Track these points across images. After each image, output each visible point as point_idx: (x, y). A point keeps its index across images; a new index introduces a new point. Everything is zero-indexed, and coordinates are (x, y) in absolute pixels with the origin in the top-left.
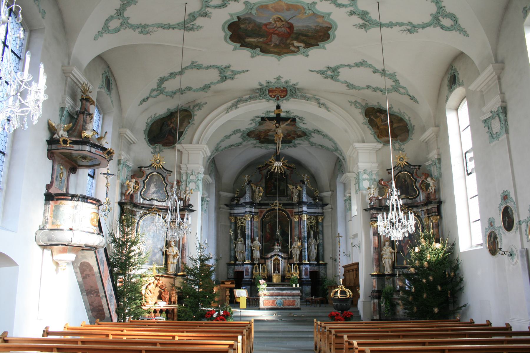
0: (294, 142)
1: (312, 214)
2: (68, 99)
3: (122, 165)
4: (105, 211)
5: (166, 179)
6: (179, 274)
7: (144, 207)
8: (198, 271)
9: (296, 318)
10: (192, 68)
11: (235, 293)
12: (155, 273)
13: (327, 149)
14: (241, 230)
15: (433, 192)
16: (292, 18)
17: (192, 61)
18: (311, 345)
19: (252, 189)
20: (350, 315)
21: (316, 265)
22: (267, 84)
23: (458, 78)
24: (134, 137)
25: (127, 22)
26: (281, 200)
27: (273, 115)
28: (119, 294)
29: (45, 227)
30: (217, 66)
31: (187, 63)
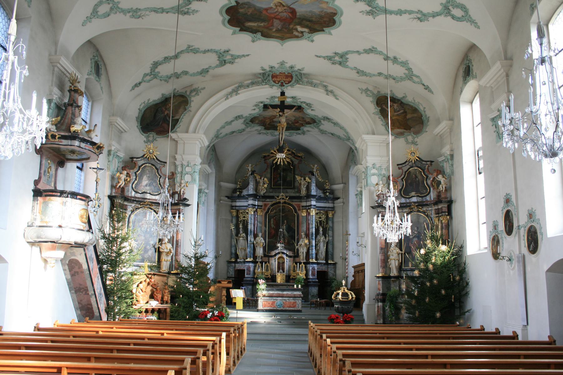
0: (303, 129)
1: (322, 209)
2: (56, 90)
3: (112, 155)
4: (95, 207)
5: (159, 170)
6: (172, 272)
7: (135, 201)
8: (192, 269)
9: (296, 321)
10: (188, 52)
11: (231, 292)
12: (147, 271)
13: (339, 137)
14: (243, 225)
15: (444, 190)
16: (294, 3)
17: (188, 45)
18: (305, 347)
19: (256, 180)
20: (350, 318)
21: (325, 264)
22: (270, 69)
23: (472, 69)
24: (124, 125)
25: (118, 6)
26: (287, 193)
27: (277, 102)
28: (109, 293)
29: (34, 224)
30: (215, 50)
31: (182, 46)
